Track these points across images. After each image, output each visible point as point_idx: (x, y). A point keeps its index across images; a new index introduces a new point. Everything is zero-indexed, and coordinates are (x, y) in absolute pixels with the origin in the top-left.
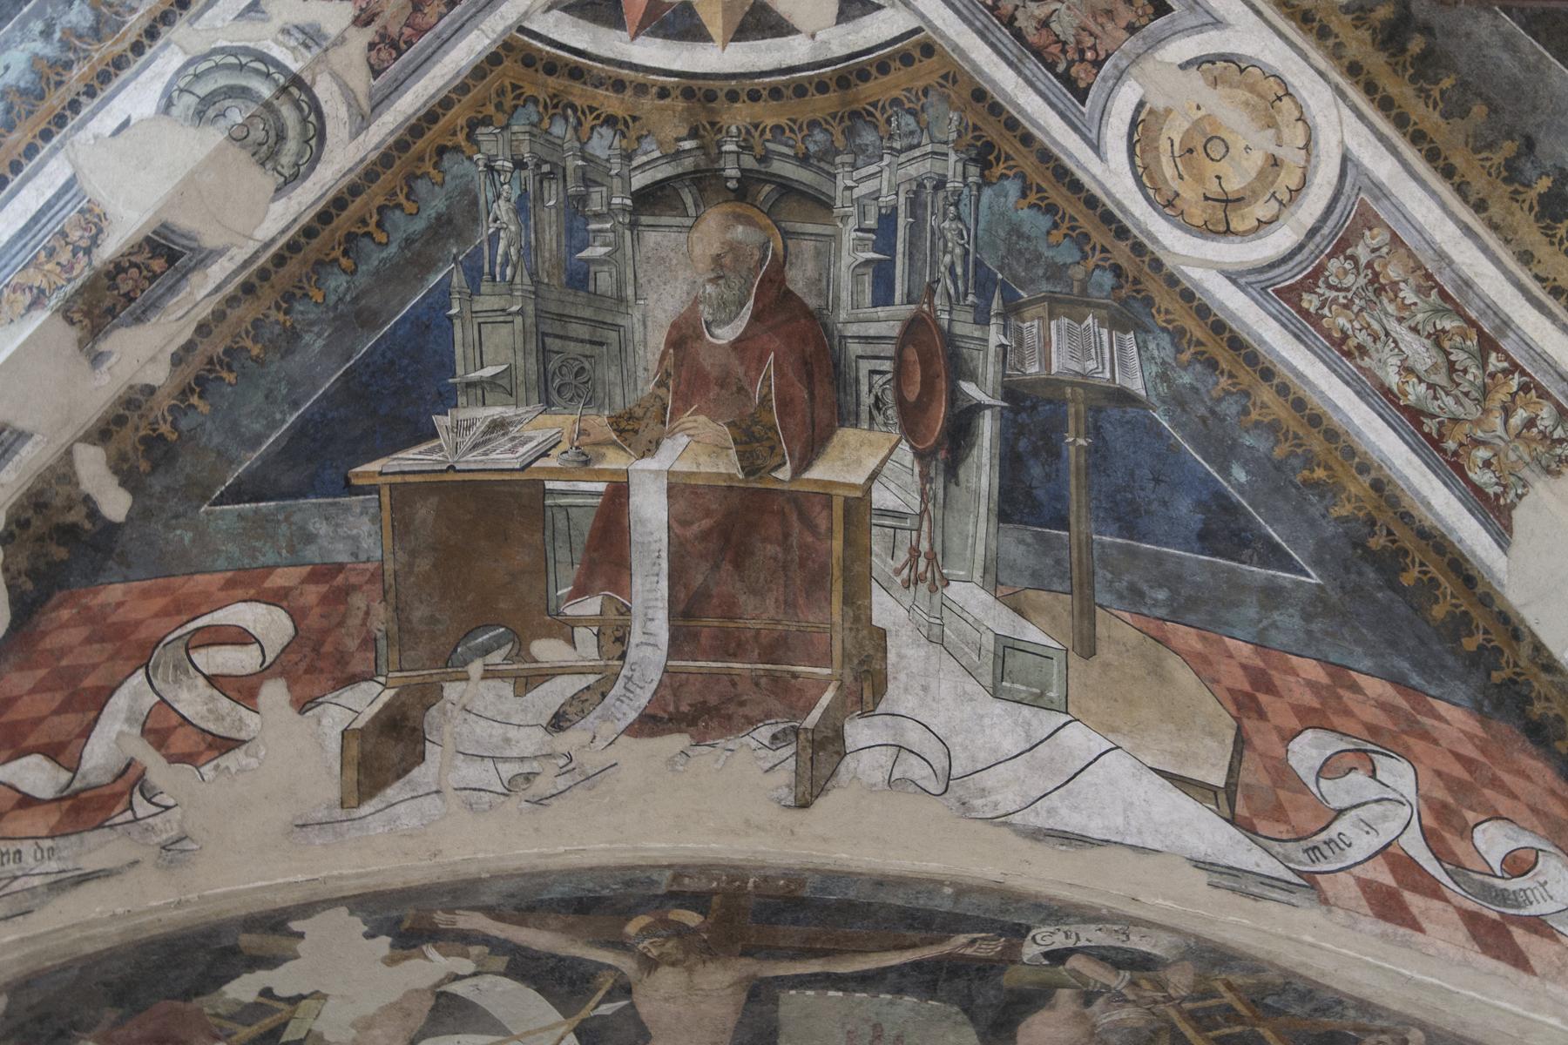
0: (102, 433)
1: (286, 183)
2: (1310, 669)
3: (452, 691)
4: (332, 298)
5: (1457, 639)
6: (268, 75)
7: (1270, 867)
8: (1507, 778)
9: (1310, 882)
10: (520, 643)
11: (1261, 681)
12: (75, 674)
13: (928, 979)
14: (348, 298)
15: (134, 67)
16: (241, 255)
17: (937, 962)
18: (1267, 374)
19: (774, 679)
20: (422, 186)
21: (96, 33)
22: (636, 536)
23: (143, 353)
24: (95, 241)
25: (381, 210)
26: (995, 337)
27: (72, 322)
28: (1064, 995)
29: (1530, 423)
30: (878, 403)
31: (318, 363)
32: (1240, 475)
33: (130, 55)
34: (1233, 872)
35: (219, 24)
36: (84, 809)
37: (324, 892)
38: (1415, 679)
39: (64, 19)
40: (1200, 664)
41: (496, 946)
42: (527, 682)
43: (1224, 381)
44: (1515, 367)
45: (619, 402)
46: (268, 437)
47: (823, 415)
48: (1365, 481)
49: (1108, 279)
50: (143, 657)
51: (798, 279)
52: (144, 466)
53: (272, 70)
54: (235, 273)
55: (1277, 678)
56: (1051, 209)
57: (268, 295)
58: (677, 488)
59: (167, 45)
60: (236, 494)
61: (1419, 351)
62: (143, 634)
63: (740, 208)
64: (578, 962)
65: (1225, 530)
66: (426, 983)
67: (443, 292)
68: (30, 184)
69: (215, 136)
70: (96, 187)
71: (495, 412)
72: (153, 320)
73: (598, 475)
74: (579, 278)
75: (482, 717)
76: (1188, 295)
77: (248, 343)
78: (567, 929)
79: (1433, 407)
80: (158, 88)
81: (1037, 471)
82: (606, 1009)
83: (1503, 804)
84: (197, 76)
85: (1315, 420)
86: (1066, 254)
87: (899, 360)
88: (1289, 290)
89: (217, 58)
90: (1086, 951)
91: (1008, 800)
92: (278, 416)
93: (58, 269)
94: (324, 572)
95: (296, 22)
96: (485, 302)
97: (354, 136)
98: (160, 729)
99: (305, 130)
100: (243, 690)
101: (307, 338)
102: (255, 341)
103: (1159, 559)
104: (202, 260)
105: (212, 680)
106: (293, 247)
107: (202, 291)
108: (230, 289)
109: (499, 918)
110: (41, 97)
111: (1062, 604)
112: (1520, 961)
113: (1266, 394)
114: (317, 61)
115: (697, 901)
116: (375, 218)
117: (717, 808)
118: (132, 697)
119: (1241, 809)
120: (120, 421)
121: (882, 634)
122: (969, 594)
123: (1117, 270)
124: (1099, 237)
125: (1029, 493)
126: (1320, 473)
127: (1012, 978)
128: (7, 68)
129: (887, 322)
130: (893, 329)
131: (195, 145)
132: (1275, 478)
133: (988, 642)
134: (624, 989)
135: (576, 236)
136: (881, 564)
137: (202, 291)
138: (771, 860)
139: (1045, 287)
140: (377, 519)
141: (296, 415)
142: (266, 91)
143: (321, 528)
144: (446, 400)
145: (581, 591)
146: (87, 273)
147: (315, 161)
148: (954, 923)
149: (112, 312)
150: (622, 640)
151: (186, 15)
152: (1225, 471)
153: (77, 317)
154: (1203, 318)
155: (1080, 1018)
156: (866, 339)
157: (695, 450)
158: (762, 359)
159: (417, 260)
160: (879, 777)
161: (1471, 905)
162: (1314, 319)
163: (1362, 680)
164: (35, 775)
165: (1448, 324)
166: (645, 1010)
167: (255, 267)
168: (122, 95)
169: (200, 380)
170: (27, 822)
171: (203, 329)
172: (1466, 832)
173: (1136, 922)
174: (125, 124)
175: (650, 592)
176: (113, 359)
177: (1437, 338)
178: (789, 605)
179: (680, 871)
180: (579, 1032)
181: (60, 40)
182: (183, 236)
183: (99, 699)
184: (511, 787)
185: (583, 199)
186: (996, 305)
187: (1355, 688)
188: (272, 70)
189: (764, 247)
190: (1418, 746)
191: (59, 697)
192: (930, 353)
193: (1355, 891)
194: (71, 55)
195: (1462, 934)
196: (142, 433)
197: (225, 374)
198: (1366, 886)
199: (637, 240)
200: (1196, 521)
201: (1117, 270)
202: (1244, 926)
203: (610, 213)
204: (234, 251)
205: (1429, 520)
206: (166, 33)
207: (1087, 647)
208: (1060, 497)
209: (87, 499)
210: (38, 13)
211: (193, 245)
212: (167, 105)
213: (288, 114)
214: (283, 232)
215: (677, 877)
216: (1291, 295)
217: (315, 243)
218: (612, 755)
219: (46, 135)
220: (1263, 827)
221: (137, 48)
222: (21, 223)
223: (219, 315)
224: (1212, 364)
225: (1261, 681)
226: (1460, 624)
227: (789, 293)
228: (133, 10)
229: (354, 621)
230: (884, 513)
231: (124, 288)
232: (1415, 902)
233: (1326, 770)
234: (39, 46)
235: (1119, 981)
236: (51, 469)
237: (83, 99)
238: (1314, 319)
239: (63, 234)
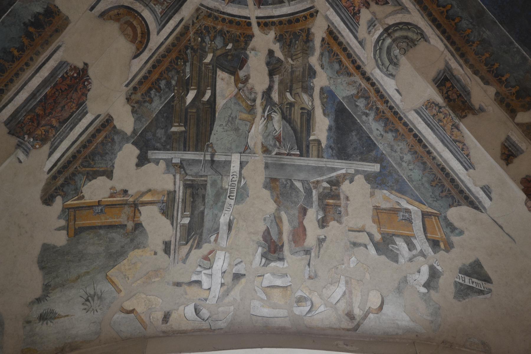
0: (512, 112)
1: (424, 38)
4: (470, 26)
6: (384, 40)
14: (471, 20)
15: (379, 86)
16: (449, 56)
21: (367, 98)
23: (481, 94)
24: (437, 105)
25: (438, 6)
27: (466, 116)
33: (375, 87)
35: (366, 55)
39: (362, 108)
46: (523, 54)
53: (382, 38)
54: (456, 59)
59: (372, 74)
68: (417, 126)
69: (403, 60)
70: (419, 103)
72: (469, 89)
77: (484, 58)
80: (386, 78)
84: (383, 64)
89: (377, 57)
92: (515, 50)
93: (446, 118)
95: (366, 29)
97: (409, 12)
99: (405, 29)
101: (485, 36)
102: (483, 55)
104: (449, 70)
106: (448, 38)
108: (461, 62)
110: (388, 119)
114: (380, 22)
116: (441, 8)
128: (377, 130)
131: (405, 65)
141: (516, 43)
142: (389, 41)
146: (447, 108)
147: (416, 27)
149: (464, 102)
151: (362, 67)
153: (464, 114)
154: (349, 58)
167: (454, 52)
168: (388, 91)
169: (496, 76)
174: (398, 91)
176: (483, 104)
181: (369, 110)
182: (438, 75)
188: (382, 38)
194: (374, 107)
196: (514, 98)
197: (495, 67)
204: (447, 58)
206: (368, 74)
210: (360, 117)
211: (442, 72)
212: (392, 76)
213: (397, 34)
214: (442, 41)
217: (448, 30)
219: (400, 119)
221: (373, 84)
222: (430, 130)
223: (471, 67)
228: (360, 85)
231: (455, 96)
234: (371, 118)
236: (523, 131)
237: (389, 105)
239: (434, 116)
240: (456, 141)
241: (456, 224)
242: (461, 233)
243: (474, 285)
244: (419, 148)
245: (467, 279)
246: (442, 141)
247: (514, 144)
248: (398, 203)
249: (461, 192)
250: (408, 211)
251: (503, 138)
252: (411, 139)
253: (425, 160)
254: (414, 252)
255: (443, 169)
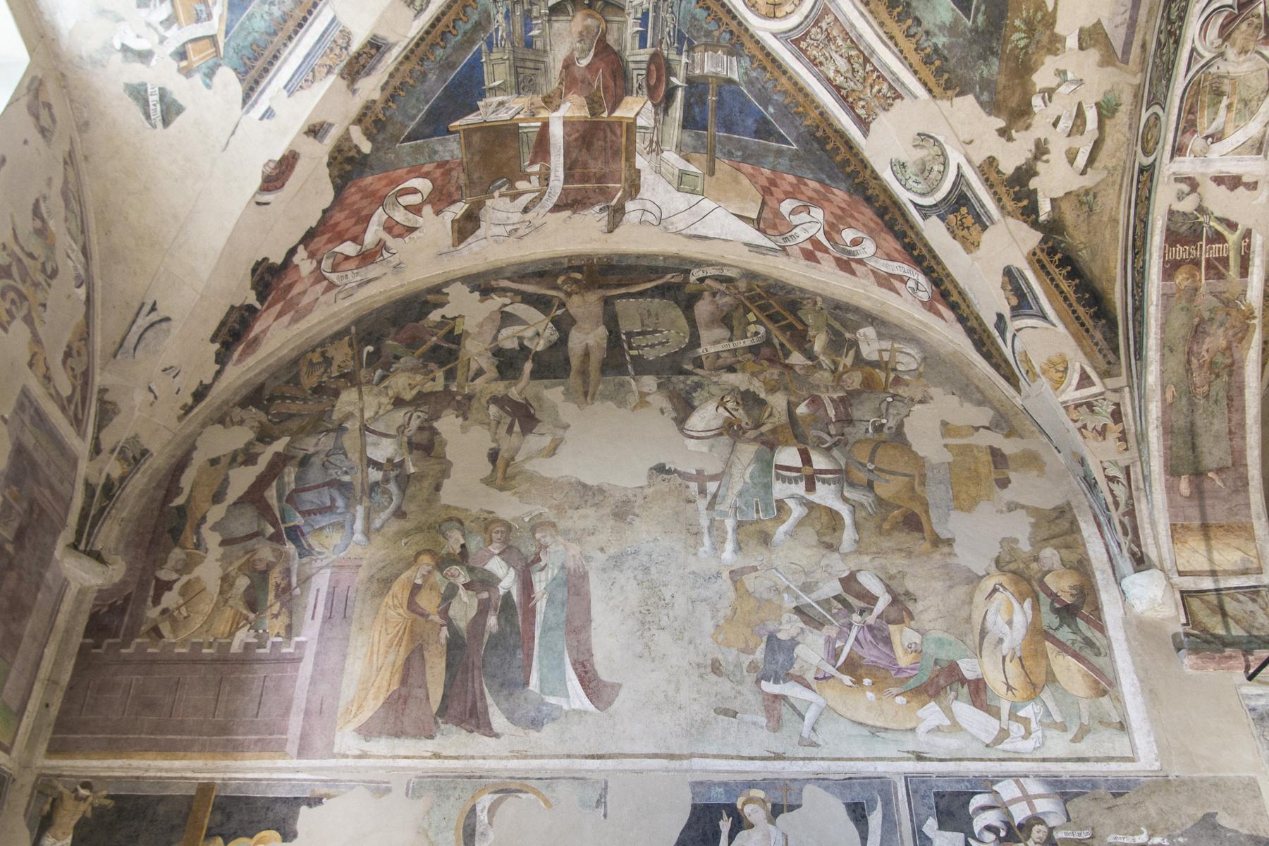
0: (359, 121)
2: (791, 178)
3: (489, 202)
5: (844, 167)
7: (770, 244)
8: (856, 215)
9: (784, 249)
10: (511, 183)
11: (773, 183)
12: (358, 211)
13: (663, 291)
16: (403, 44)
17: (663, 285)
18: (785, 72)
19: (601, 189)
20: (469, 10)
22: (552, 141)
23: (371, 87)
25: (454, 21)
26: (684, 59)
28: (706, 294)
29: (879, 91)
30: (640, 87)
31: (435, 86)
32: (771, 110)
34: (757, 246)
36: (367, 258)
37: (451, 277)
38: (828, 182)
40: (751, 177)
41: (517, 292)
42: (514, 197)
43: (768, 75)
44: (875, 69)
45: (546, 90)
47: (619, 91)
48: (817, 112)
49: (727, 36)
50: (381, 202)
51: (611, 40)
52: (375, 131)
55: (778, 181)
56: (708, 8)
57: (414, 59)
58: (567, 123)
60: (408, 139)
61: (842, 64)
62: (381, 193)
63: (591, 12)
64: (544, 296)
65: (764, 130)
66: (496, 308)
67: (479, 51)
70: (346, 21)
71: (500, 98)
73: (538, 120)
74: (529, 44)
75: (500, 210)
76: (757, 42)
78: (538, 283)
79: (845, 85)
81: (697, 110)
82: (559, 312)
83: (853, 223)
85: (801, 89)
86: (712, 26)
87: (648, 70)
88: (796, 41)
90: (712, 277)
91: (681, 226)
94: (441, 165)
96: (495, 56)
98: (390, 227)
100: (416, 210)
103: (740, 141)
105: (406, 207)
106: (422, 39)
107: (390, 60)
109: (513, 281)
111: (703, 158)
112: (853, 273)
113: (784, 80)
115: (578, 269)
117: (582, 235)
118: (379, 216)
119: (762, 226)
120: (364, 115)
121: (639, 171)
122: (671, 156)
123: (731, 32)
124: (726, 19)
125: (694, 118)
126: (801, 109)
127: (688, 289)
129: (644, 54)
130: (646, 58)
132: (784, 111)
133: (676, 172)
134: (562, 305)
135: (528, 26)
136: (639, 146)
137: (390, 60)
138: (600, 251)
139: (704, 39)
140: (459, 143)
143: (439, 148)
144: (482, 95)
145: (532, 163)
148: (666, 270)
149: (358, 73)
150: (547, 179)
152: (766, 109)
155: (713, 302)
156: (636, 62)
157: (573, 108)
158: (597, 72)
159: (469, 41)
160: (637, 221)
161: (838, 255)
162: (804, 51)
163: (808, 182)
164: (349, 248)
165: (853, 53)
166: (571, 311)
169: (392, 96)
170: (347, 265)
171: (391, 75)
172: (839, 232)
173: (725, 265)
175: (557, 161)
177: (849, 59)
178: (607, 163)
179: (570, 258)
180: (552, 321)
183: (368, 218)
184: (510, 234)
185: (530, 11)
186: (685, 47)
187: (806, 184)
189: (598, 27)
190: (826, 204)
191: (353, 220)
192: (660, 66)
193: (798, 251)
195: (834, 264)
198: (804, 251)
199: (550, 27)
200: (754, 127)
201: (731, 32)
202: (758, 264)
203: (541, 16)
205: (839, 127)
207: (711, 172)
208: (705, 119)
209: (356, 146)
215: (570, 261)
216: (796, 42)
218: (545, 219)
220: (769, 231)
223: (397, 69)
224: (765, 69)
225: (773, 183)
226: (847, 162)
227: (608, 45)
229: (453, 181)
230: (641, 127)
232: (819, 254)
233: (792, 212)
235: (723, 287)
238: (804, 51)
240: (313, 71)
241: (216, 79)
242: (209, 86)
243: (152, 107)
244: (291, 25)
245: (156, 98)
246: (308, 55)
247: (327, 131)
248: (215, 3)
249: (257, 82)
250: (210, 16)
251: (330, 121)
252: (299, 14)
253: (280, 34)
254: (161, 29)
255: (276, 57)
